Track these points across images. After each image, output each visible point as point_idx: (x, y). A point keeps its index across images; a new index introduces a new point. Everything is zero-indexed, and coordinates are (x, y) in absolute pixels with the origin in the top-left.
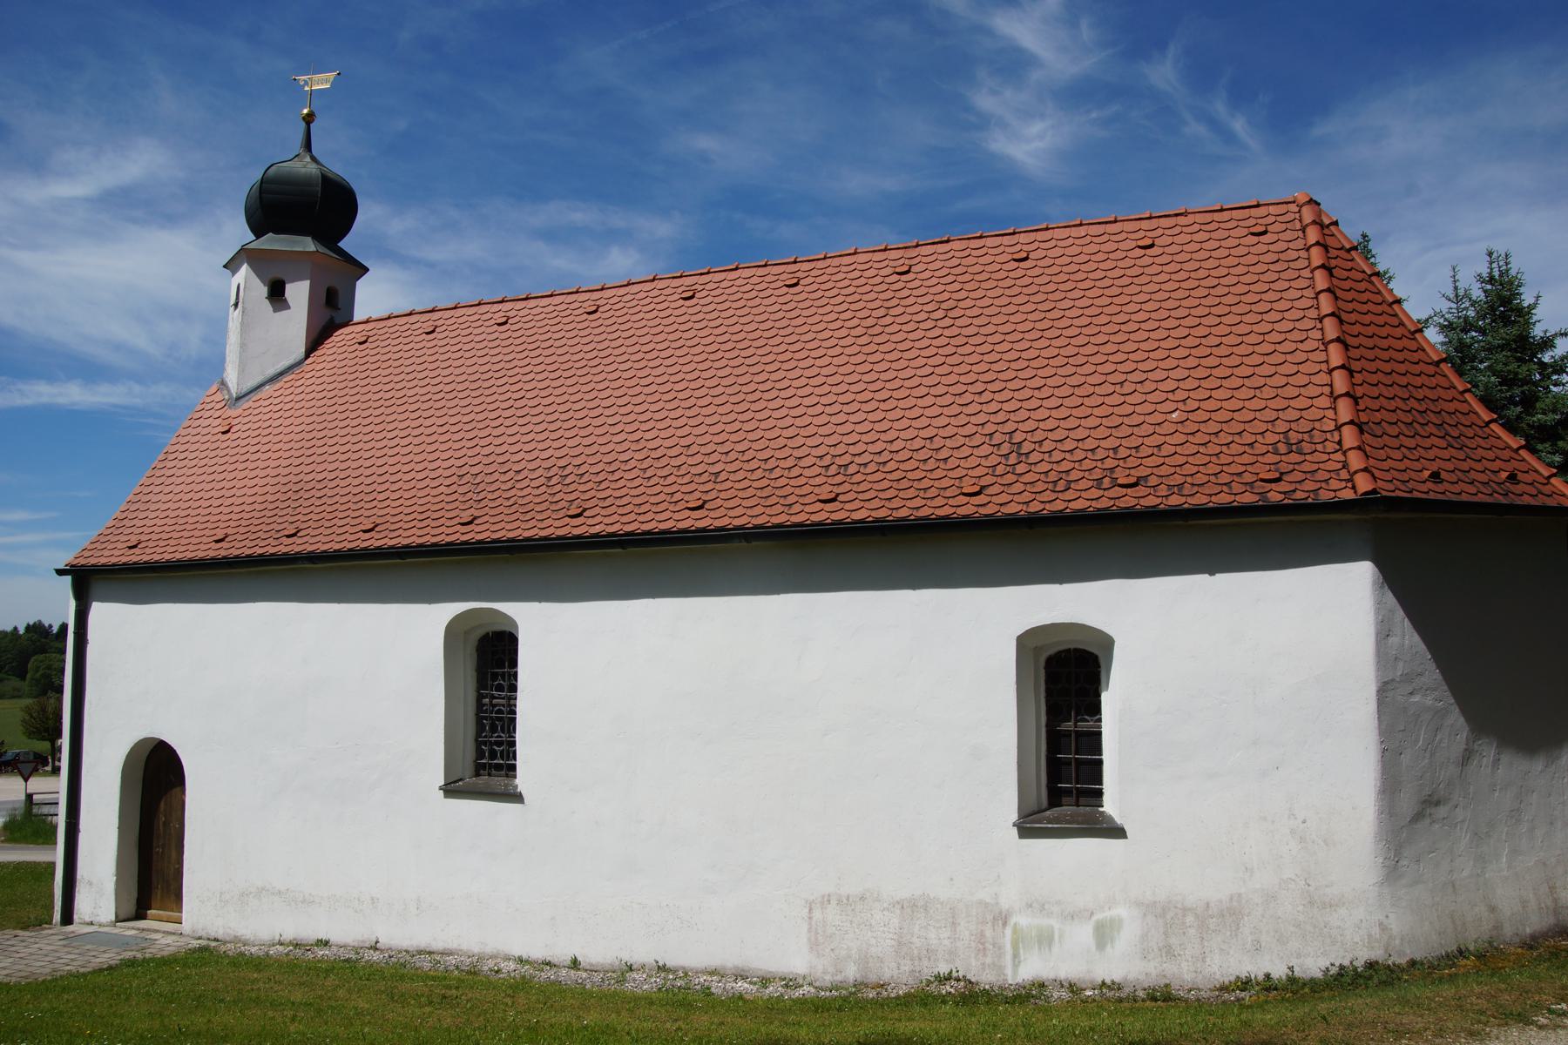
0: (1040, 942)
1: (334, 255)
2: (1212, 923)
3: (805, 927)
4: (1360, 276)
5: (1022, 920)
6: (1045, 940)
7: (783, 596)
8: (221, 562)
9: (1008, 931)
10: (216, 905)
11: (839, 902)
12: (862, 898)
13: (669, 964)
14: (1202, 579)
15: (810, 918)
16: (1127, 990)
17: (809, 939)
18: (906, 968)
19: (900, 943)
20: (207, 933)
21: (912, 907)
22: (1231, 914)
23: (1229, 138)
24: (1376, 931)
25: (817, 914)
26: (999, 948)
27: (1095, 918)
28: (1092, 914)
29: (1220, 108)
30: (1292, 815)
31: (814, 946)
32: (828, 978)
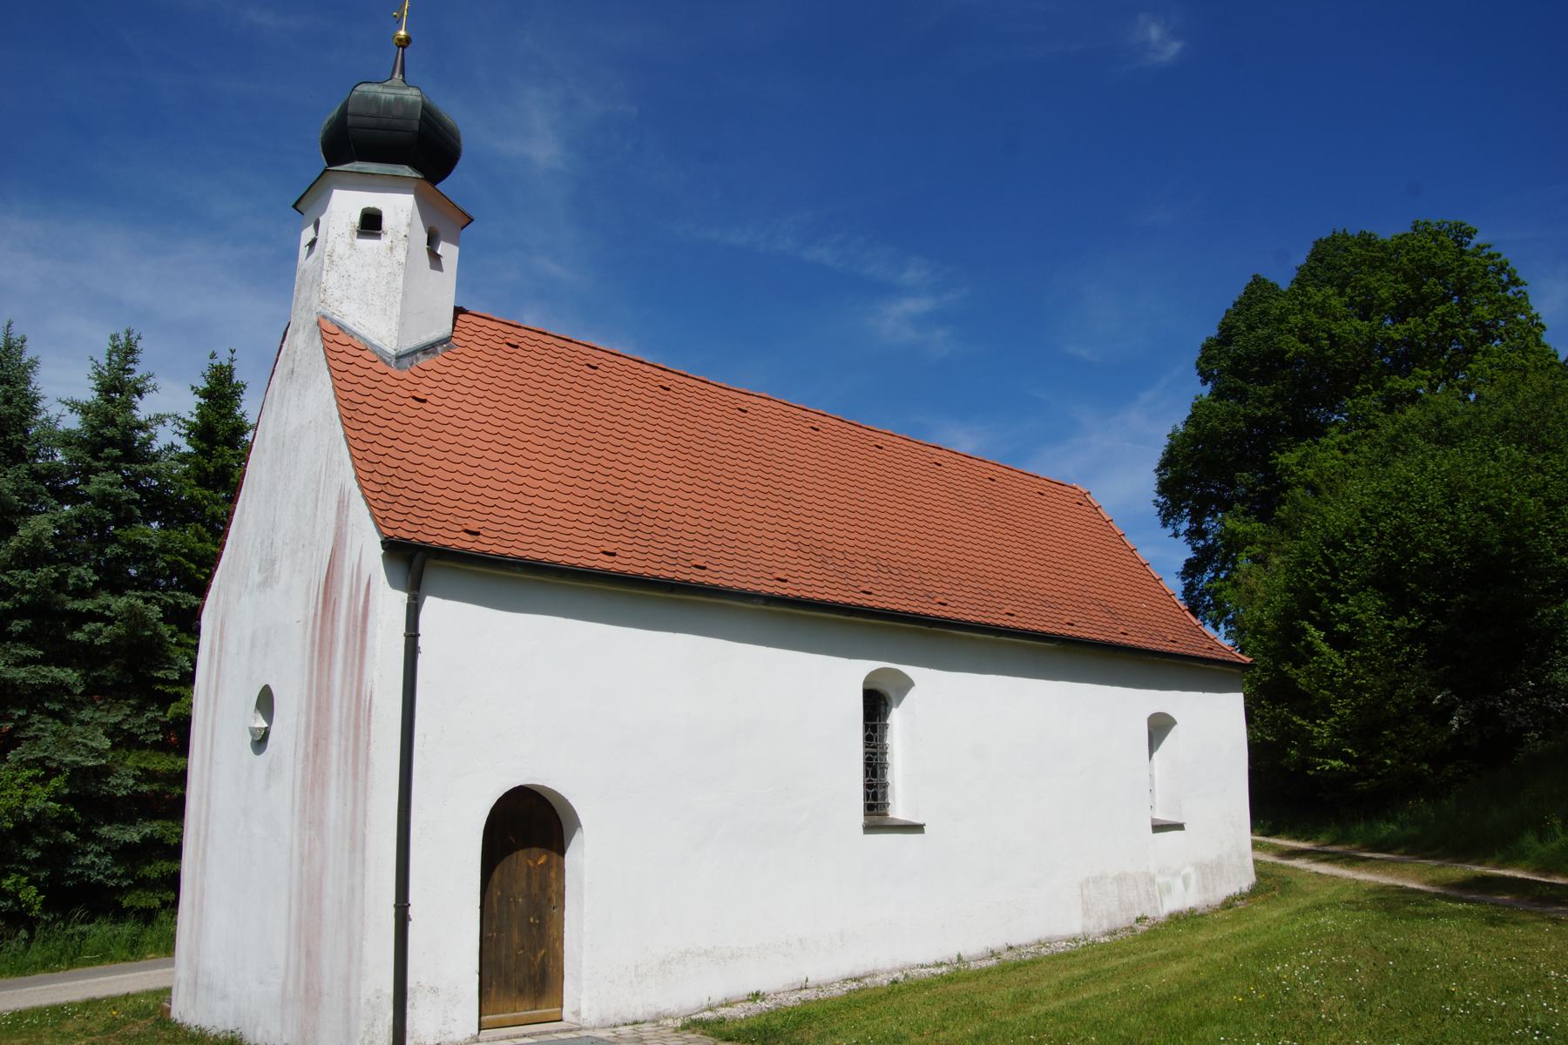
1: (1384, 856)
4: (1178, 611)
6: (1169, 889)
8: (547, 567)
21: (1120, 879)
25: (1086, 892)
31: (1086, 912)
32: (1096, 931)
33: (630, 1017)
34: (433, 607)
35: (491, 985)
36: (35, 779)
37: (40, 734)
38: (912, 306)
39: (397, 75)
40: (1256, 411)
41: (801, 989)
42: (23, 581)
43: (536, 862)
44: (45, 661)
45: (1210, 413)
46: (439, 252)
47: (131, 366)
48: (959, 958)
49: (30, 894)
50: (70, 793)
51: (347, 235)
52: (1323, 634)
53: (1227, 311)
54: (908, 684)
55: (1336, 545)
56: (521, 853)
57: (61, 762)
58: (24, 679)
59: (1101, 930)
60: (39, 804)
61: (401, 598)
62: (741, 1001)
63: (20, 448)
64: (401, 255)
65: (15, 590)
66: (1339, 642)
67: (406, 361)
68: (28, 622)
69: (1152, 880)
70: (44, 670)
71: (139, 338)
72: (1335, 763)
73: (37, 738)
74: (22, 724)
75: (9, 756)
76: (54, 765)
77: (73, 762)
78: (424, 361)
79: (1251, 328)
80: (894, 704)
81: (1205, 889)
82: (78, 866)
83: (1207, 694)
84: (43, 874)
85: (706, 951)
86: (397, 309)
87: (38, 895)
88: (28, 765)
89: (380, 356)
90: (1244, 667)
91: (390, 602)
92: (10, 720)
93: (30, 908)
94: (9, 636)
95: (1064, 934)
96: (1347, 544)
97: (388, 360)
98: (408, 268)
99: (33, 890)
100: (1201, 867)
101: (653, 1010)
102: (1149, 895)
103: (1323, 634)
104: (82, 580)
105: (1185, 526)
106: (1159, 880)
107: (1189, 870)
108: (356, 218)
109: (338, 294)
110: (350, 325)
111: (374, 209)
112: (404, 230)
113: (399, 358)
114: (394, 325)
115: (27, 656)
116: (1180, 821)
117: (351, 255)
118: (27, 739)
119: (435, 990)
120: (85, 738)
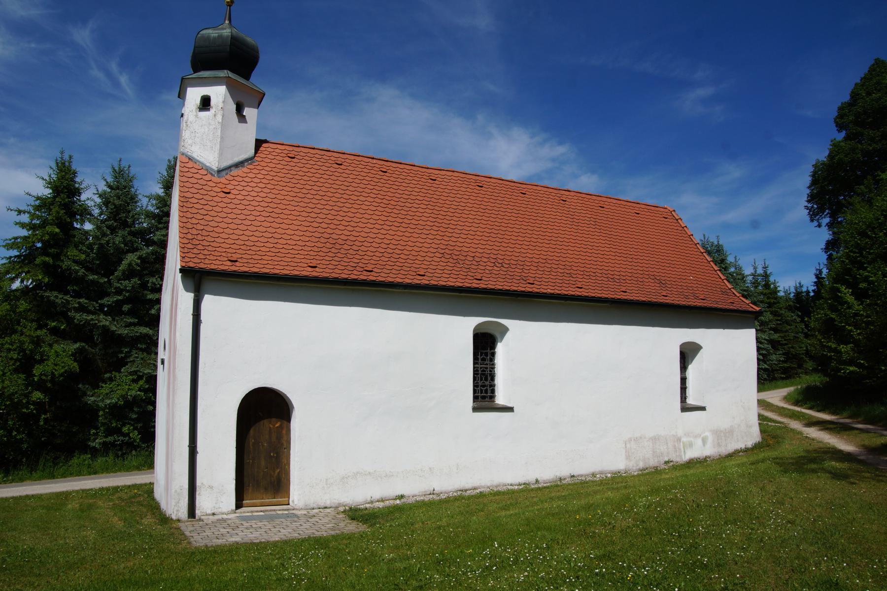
0: (690, 447)
3: (624, 451)
4: (719, 280)
5: (684, 439)
6: (691, 445)
9: (682, 444)
12: (641, 438)
13: (575, 475)
14: (721, 330)
15: (626, 447)
16: (711, 458)
17: (626, 455)
18: (656, 461)
19: (654, 452)
20: (318, 505)
21: (655, 439)
22: (730, 432)
23: (117, 84)
25: (628, 446)
26: (680, 449)
27: (702, 436)
29: (114, 67)
31: (628, 458)
32: (634, 468)
33: (322, 505)
34: (209, 302)
35: (249, 486)
36: (134, 381)
38: (702, 92)
39: (227, 22)
40: (869, 147)
41: (430, 494)
43: (274, 426)
44: (139, 324)
45: (839, 150)
46: (244, 114)
48: (537, 481)
50: (149, 387)
52: (850, 291)
53: (856, 84)
54: (505, 330)
55: (863, 234)
56: (266, 422)
57: (144, 373)
59: (638, 468)
60: (133, 393)
61: (190, 296)
62: (392, 499)
64: (219, 118)
65: (122, 290)
66: (860, 295)
67: (224, 173)
68: (129, 306)
69: (679, 440)
70: (136, 329)
72: (851, 368)
73: (134, 361)
75: (122, 370)
76: (141, 374)
78: (235, 172)
79: (869, 94)
80: (499, 339)
81: (719, 445)
84: (139, 425)
85: (369, 473)
87: (138, 435)
88: (131, 374)
89: (208, 170)
90: (757, 314)
91: (187, 299)
92: (123, 353)
94: (123, 313)
96: (869, 233)
97: (214, 173)
98: (224, 125)
99: (136, 433)
100: (717, 433)
101: (337, 502)
102: (675, 448)
103: (850, 291)
104: (154, 284)
105: (827, 220)
106: (684, 439)
107: (707, 434)
109: (190, 142)
110: (196, 157)
111: (207, 96)
112: (221, 105)
114: (216, 154)
115: (131, 322)
116: (703, 405)
117: (196, 121)
118: (131, 362)
119: (211, 487)
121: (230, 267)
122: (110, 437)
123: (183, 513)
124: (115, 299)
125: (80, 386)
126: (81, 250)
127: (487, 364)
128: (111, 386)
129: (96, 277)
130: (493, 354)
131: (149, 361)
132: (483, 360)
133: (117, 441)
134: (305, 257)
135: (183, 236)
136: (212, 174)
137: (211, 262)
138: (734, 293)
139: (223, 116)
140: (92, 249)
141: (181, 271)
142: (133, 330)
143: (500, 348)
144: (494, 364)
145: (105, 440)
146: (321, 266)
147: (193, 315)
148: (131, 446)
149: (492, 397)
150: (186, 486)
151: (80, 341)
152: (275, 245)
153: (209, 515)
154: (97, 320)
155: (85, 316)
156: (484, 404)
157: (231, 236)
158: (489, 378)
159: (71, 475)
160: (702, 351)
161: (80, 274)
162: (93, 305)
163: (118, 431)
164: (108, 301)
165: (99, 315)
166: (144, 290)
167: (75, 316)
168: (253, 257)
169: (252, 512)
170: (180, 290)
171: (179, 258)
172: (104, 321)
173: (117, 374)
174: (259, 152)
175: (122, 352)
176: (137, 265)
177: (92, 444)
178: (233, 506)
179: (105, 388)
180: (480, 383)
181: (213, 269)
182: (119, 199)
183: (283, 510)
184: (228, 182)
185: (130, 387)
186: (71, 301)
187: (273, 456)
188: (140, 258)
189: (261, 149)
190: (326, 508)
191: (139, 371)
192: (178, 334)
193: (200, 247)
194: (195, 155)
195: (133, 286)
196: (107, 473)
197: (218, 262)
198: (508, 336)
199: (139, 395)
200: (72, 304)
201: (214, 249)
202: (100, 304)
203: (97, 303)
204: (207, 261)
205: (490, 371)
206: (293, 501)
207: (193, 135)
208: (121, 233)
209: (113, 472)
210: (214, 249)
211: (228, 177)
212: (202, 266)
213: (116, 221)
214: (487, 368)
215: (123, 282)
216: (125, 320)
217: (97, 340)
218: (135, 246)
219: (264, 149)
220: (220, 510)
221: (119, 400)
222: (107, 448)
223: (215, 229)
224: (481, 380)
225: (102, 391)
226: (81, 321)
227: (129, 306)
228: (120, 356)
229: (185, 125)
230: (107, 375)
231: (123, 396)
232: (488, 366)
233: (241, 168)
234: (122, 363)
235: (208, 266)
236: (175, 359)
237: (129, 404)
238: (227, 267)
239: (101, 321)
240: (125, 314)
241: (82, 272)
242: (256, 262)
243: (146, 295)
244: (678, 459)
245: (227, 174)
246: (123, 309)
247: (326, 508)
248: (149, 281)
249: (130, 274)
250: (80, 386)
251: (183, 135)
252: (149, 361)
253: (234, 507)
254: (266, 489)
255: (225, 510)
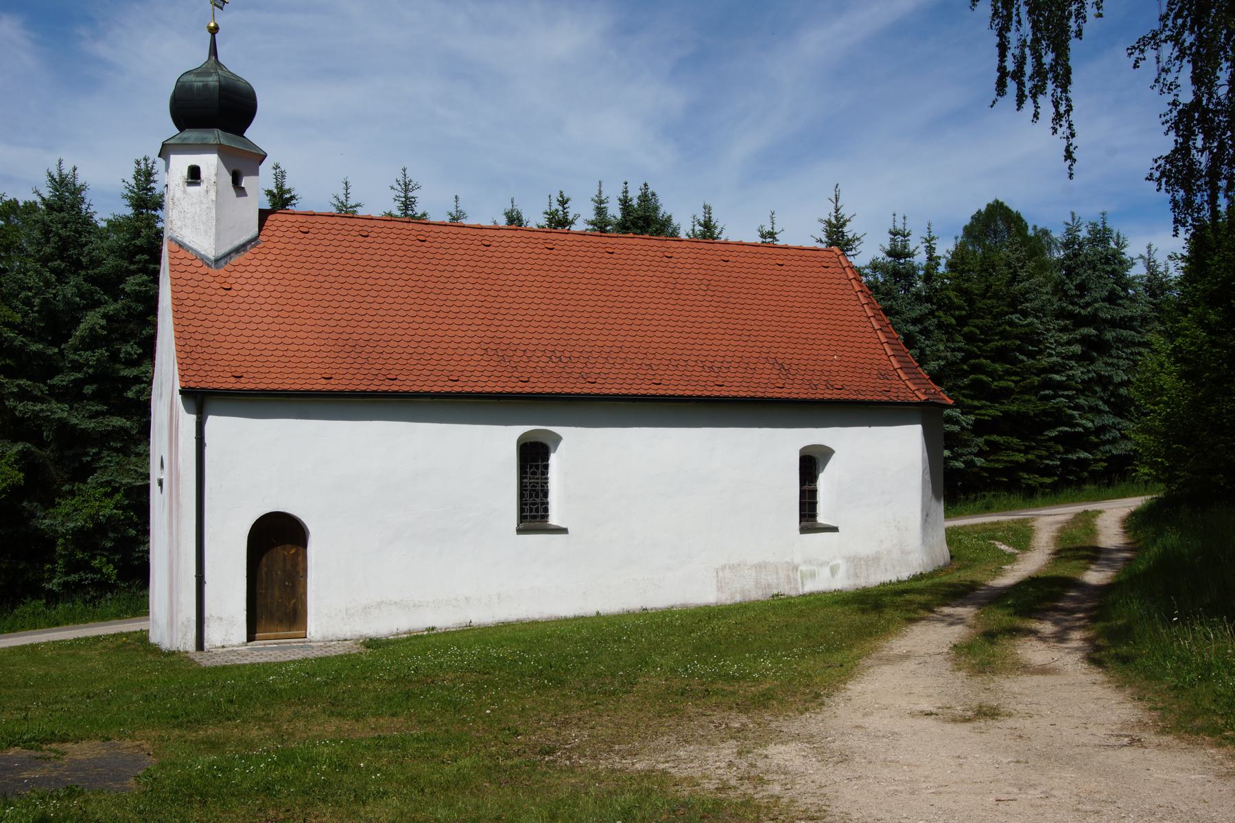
2: (870, 562)
5: (803, 568)
6: (813, 575)
7: (703, 429)
9: (799, 573)
10: (343, 618)
11: (730, 568)
12: (739, 565)
18: (761, 593)
21: (760, 567)
22: (875, 559)
24: (921, 561)
25: (721, 574)
26: (796, 580)
28: (828, 563)
30: (895, 520)
33: (342, 637)
34: (214, 423)
35: (262, 618)
36: (106, 495)
37: (108, 464)
42: (87, 360)
43: (289, 552)
44: (111, 413)
46: (243, 185)
47: (152, 185)
48: (598, 613)
49: (109, 569)
51: (181, 184)
54: (557, 439)
56: (279, 549)
58: (94, 428)
60: (107, 511)
63: (78, 259)
64: (213, 195)
67: (222, 262)
68: (94, 387)
69: (796, 568)
71: (154, 163)
73: (106, 467)
74: (96, 457)
75: (89, 480)
76: (117, 485)
77: (128, 483)
78: (236, 259)
80: (552, 450)
82: (139, 551)
83: (873, 428)
84: (117, 557)
85: (395, 602)
86: (213, 230)
87: (114, 569)
88: (102, 485)
89: (203, 259)
93: (109, 578)
95: (698, 602)
97: (210, 263)
98: (218, 204)
99: (111, 566)
104: (130, 354)
106: (803, 568)
108: (185, 173)
109: (179, 224)
110: (188, 243)
112: (213, 179)
113: (217, 261)
114: (212, 240)
115: (97, 411)
116: (835, 525)
117: (184, 198)
118: (101, 468)
119: (220, 619)
120: (137, 466)
121: (235, 385)
122: (73, 575)
123: (191, 645)
124: (72, 378)
125: (25, 504)
126: (16, 307)
127: (538, 479)
128: (73, 502)
129: (41, 346)
130: (546, 467)
131: (128, 467)
132: (534, 473)
133: (85, 580)
134: (320, 365)
135: (180, 336)
136: (208, 265)
137: (213, 379)
138: (899, 376)
139: (217, 193)
140: (31, 305)
141: (181, 392)
142: (102, 422)
143: (554, 460)
144: (547, 479)
145: (66, 579)
146: (337, 376)
147: (197, 438)
148: (103, 586)
149: (545, 516)
150: (194, 618)
151: (23, 440)
152: (285, 353)
153: (219, 648)
154: (48, 410)
155: (30, 406)
156: (532, 524)
157: (234, 345)
158: (541, 495)
159: (23, 628)
160: (834, 455)
161: (17, 343)
162: (39, 389)
163: (85, 566)
164: (62, 381)
165: (49, 402)
166: (114, 364)
167: (16, 406)
168: (260, 370)
169: (265, 644)
170: (180, 412)
171: (177, 377)
172: (60, 411)
173: (81, 486)
174: (265, 228)
175: (87, 454)
176: (102, 327)
177: (48, 586)
178: (243, 636)
179: (66, 506)
180: (529, 501)
181: (215, 389)
182: (66, 227)
183: (299, 642)
184: (228, 274)
185: (103, 504)
186: (7, 383)
187: (288, 586)
188: (105, 316)
189: (268, 223)
190: (346, 640)
191: (114, 481)
192: (180, 459)
193: (200, 362)
194: (186, 241)
195: (98, 360)
196: (74, 623)
197: (221, 380)
198: (562, 445)
199: (116, 514)
200: (8, 389)
201: (216, 363)
202: (50, 386)
203: (45, 384)
204: (209, 379)
205: (542, 486)
206: (310, 634)
207: (183, 215)
208: (73, 280)
209: (82, 622)
210: (216, 363)
211: (228, 267)
212: (203, 385)
213: (63, 259)
214: (538, 483)
215: (82, 352)
216: (88, 407)
217: (48, 436)
218: (96, 298)
219: (271, 223)
220: (230, 643)
221: (86, 522)
222: (70, 590)
223: (218, 351)
224: (531, 497)
225: (59, 510)
226: (26, 413)
227: (94, 387)
228: (85, 459)
229: (171, 203)
230: (66, 488)
231: (92, 517)
232: (539, 481)
233: (242, 253)
234: (88, 470)
235: (211, 384)
236: (178, 485)
237: (101, 528)
238: (232, 384)
239: (55, 413)
240: (88, 399)
241: (19, 340)
242: (264, 376)
243: (119, 370)
244: (793, 593)
245: (226, 264)
246: (85, 391)
247: (346, 640)
248: (120, 349)
249: (92, 342)
250: (25, 504)
251: (170, 215)
252: (128, 467)
253: (245, 640)
254: (281, 621)
255: (235, 643)
